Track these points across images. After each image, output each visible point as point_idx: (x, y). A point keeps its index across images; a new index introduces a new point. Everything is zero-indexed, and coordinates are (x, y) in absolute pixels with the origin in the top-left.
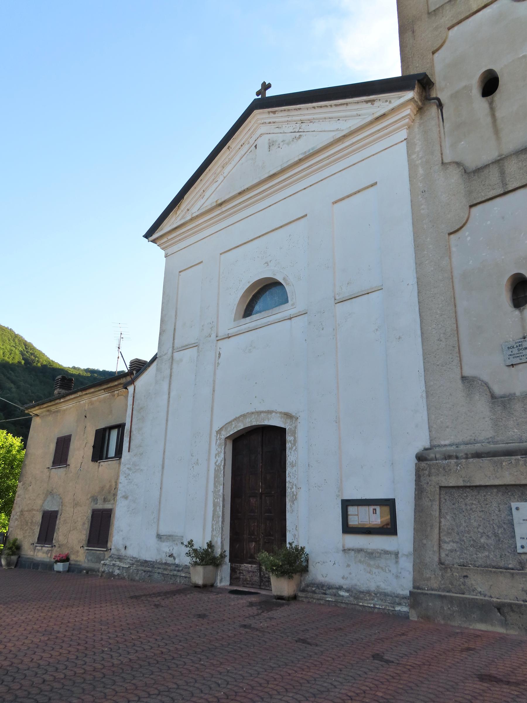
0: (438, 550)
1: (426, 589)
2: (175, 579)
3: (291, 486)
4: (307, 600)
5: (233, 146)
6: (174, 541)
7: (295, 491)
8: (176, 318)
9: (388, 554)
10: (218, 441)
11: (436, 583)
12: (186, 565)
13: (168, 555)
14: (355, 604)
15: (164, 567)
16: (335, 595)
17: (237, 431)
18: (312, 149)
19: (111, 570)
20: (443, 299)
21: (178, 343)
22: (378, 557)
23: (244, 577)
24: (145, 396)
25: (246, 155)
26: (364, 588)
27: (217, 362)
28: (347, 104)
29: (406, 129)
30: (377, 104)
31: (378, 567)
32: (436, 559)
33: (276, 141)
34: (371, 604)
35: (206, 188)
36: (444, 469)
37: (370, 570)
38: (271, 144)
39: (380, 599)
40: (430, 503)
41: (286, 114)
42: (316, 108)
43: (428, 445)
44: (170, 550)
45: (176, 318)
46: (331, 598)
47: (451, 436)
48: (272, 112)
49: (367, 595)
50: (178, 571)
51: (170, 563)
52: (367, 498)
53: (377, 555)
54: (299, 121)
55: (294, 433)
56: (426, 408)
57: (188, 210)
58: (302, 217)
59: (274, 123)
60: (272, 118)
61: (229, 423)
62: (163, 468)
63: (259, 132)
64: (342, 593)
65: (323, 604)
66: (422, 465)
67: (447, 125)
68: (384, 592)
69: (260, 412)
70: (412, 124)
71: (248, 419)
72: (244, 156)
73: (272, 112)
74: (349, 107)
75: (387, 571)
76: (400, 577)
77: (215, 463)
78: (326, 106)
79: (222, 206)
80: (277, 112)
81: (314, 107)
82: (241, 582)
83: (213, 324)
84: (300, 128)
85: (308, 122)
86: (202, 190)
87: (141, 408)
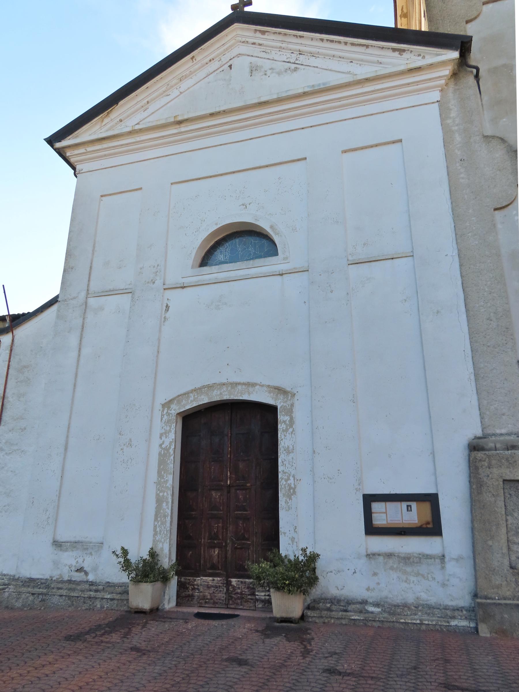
0: (507, 552)
1: (497, 598)
2: (93, 603)
3: (286, 477)
4: (322, 620)
5: (198, 58)
7: (293, 483)
8: (93, 254)
9: (431, 558)
10: (166, 417)
11: (509, 590)
12: (108, 582)
13: (73, 569)
14: (393, 622)
15: (66, 586)
16: (361, 612)
17: (197, 405)
18: (324, 84)
20: (492, 276)
21: (95, 286)
22: (417, 563)
23: (201, 594)
24: (32, 351)
25: (216, 73)
26: (398, 600)
27: (163, 316)
28: (367, 46)
29: (439, 91)
30: (405, 55)
31: (418, 574)
32: (506, 562)
33: (262, 67)
34: (416, 620)
35: (152, 100)
36: (507, 460)
37: (407, 579)
38: (253, 70)
39: (426, 613)
40: (494, 499)
41: (280, 38)
42: (325, 41)
43: (479, 433)
44: (77, 562)
45: (93, 254)
46: (359, 616)
47: (508, 424)
48: (260, 31)
49: (406, 609)
50: (96, 591)
52: (398, 493)
53: (416, 560)
54: (297, 51)
55: (290, 412)
56: (475, 392)
57: (121, 121)
58: (136, 190)
59: (260, 45)
60: (259, 38)
61: (185, 394)
62: (66, 449)
63: (236, 51)
64: (371, 609)
65: (346, 624)
66: (479, 456)
67: (485, 98)
68: (426, 604)
69: (236, 384)
70: (446, 87)
71: (215, 391)
72: (211, 73)
73: (260, 31)
74: (370, 51)
75: (431, 579)
76: (447, 585)
77: (161, 445)
78: (340, 42)
79: (182, 125)
80: (267, 34)
81: (322, 40)
82: (195, 601)
83: (159, 267)
84: (297, 60)
85: (309, 55)
86: (147, 100)
87: (25, 367)
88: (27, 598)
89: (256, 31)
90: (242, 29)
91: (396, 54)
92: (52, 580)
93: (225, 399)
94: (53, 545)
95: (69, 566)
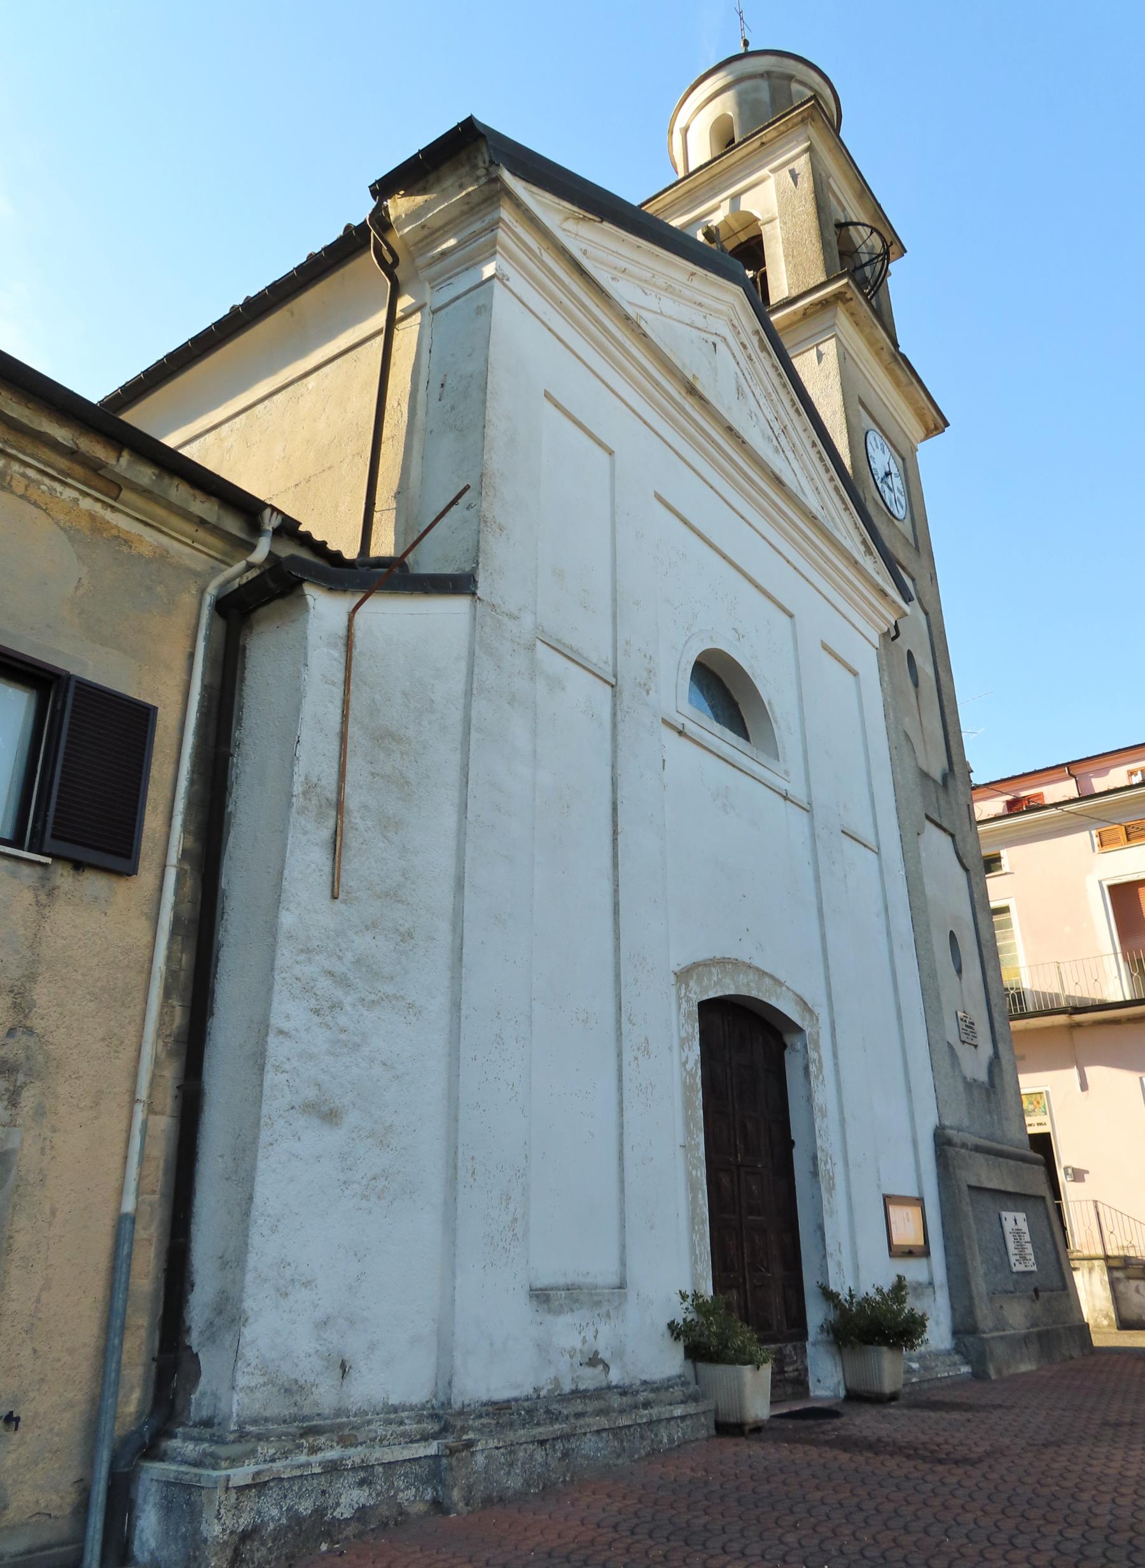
2: (656, 1435)
5: (695, 283)
6: (598, 1304)
10: (684, 1005)
13: (578, 1358)
19: (305, 1507)
28: (846, 509)
44: (584, 1341)
51: (591, 1387)
74: (845, 515)
79: (689, 398)
88: (531, 1456)
89: (757, 332)
90: (743, 306)
91: (862, 549)
92: (538, 1397)
93: (753, 996)
94: (531, 1297)
95: (569, 1352)
